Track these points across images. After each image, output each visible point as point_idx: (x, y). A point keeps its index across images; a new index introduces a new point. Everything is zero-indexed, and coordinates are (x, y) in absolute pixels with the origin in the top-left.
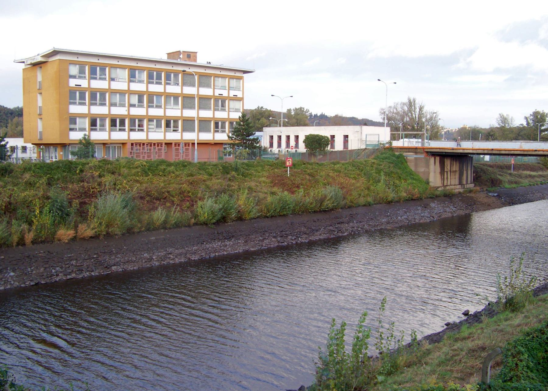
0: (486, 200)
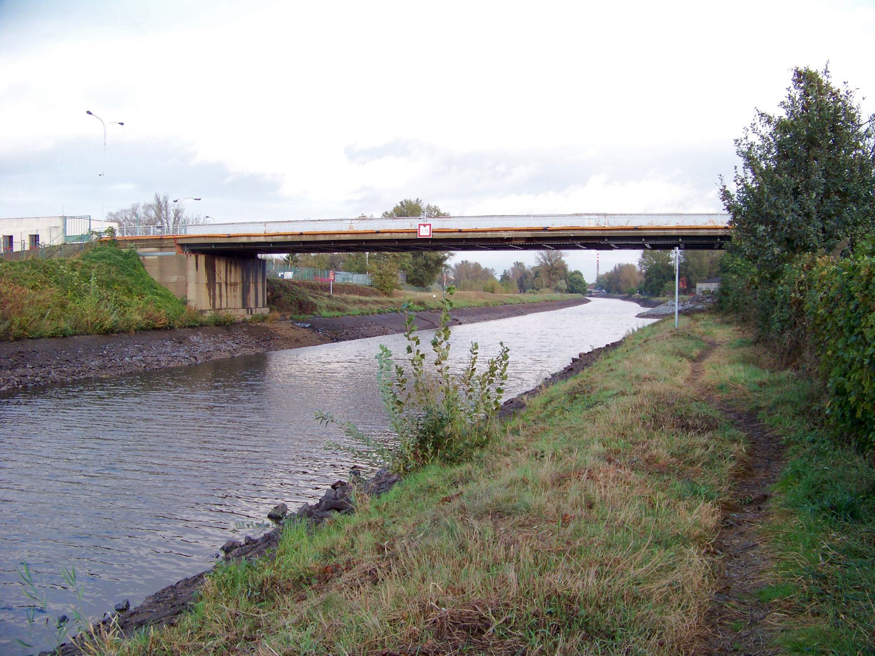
0: (291, 333)
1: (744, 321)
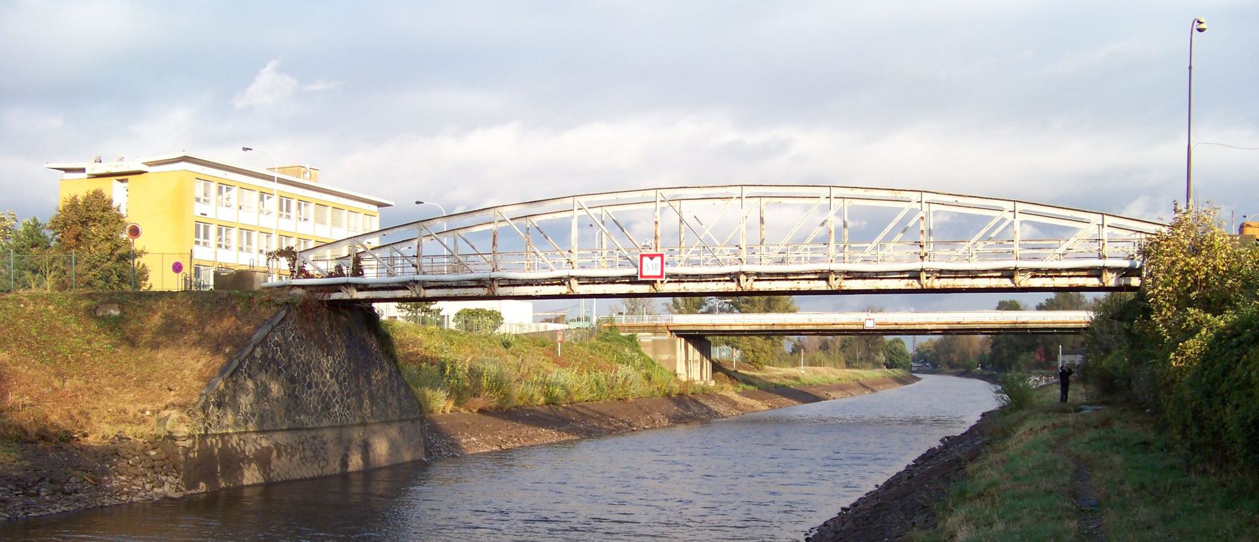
1: (390, 455)
